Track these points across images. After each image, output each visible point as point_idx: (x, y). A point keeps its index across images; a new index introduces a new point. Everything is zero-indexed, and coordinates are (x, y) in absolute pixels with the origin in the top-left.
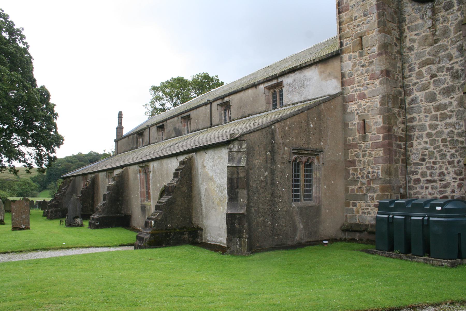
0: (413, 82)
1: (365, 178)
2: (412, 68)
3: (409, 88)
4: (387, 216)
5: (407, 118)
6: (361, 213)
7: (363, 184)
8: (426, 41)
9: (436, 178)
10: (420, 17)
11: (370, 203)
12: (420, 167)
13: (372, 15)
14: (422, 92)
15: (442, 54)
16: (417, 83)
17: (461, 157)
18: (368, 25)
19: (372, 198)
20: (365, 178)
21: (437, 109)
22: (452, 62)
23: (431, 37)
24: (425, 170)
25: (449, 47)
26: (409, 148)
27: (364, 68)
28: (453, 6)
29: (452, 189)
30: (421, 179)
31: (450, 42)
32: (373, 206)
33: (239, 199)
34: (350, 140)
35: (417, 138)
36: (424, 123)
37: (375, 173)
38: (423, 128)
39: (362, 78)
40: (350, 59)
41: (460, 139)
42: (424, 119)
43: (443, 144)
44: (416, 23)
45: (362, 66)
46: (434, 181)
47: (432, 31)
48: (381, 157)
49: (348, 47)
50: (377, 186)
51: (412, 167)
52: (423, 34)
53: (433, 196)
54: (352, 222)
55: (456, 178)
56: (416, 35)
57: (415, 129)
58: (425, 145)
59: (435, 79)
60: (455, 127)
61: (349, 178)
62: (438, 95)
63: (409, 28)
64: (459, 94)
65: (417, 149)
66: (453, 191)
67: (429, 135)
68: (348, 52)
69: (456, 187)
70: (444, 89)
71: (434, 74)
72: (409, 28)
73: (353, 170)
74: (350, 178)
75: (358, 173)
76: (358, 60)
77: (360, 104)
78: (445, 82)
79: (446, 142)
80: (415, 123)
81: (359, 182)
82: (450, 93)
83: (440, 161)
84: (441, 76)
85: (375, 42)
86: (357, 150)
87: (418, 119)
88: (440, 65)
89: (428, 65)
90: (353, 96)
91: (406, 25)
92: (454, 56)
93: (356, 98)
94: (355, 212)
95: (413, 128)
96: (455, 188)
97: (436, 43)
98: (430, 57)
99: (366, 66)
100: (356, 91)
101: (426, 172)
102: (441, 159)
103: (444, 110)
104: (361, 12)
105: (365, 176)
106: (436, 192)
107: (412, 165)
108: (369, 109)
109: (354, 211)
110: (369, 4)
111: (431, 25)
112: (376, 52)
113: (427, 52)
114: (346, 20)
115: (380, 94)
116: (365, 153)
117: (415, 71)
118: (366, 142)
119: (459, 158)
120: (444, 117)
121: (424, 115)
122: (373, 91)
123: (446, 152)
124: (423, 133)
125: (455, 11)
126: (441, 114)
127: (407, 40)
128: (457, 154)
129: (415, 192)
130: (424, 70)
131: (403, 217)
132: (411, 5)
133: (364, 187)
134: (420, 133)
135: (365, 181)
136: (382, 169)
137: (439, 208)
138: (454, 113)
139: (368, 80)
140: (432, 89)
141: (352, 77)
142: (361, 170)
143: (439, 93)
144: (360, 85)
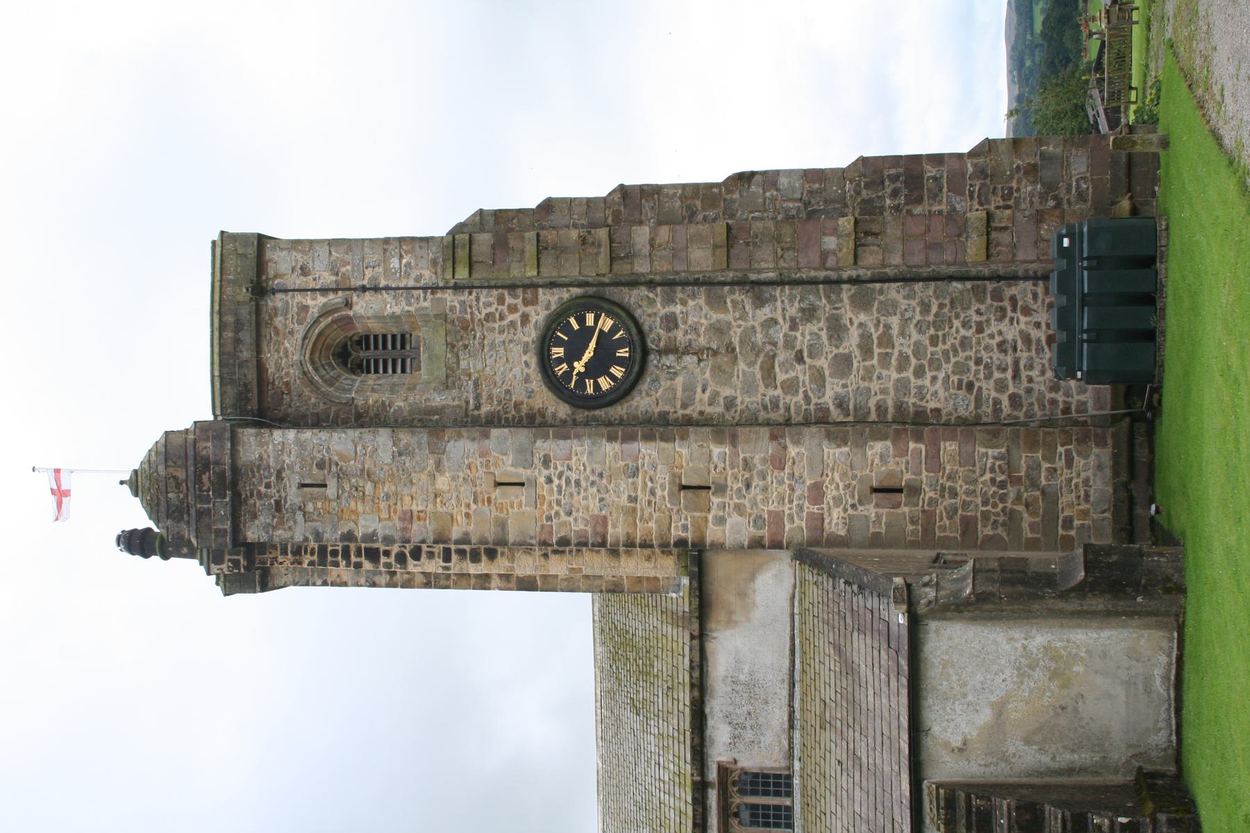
0: (802, 402)
1: (1005, 491)
2: (771, 403)
3: (813, 412)
4: (1085, 345)
5: (876, 420)
6: (1088, 506)
7: (1018, 498)
8: (724, 370)
9: (1009, 359)
10: (672, 379)
11: (1063, 478)
12: (985, 393)
13: (641, 455)
14: (827, 384)
15: (759, 338)
16: (805, 393)
17: (969, 308)
18: (659, 467)
19: (1051, 474)
20: (1005, 491)
21: (869, 354)
22: (780, 320)
23: (719, 359)
24: (992, 382)
25: (749, 324)
26: (941, 418)
27: (754, 484)
28: (674, 313)
29: (1032, 327)
30: (1010, 392)
31: (740, 322)
32: (1069, 471)
33: (1049, 571)
34: (912, 531)
35: (922, 399)
36: (892, 383)
37: (994, 464)
38: (902, 385)
39: (774, 490)
40: (721, 521)
41: (934, 309)
42: (883, 381)
43: (940, 343)
44: (680, 389)
45: (748, 486)
46: (1016, 363)
47: (707, 356)
48: (959, 448)
49: (692, 525)
50: (1023, 461)
51: (985, 412)
52: (708, 375)
53: (1047, 365)
54: (1109, 531)
55: (1012, 319)
56: (704, 391)
57: (902, 403)
58: (940, 382)
59: (805, 354)
60: (909, 318)
61: (1003, 538)
62: (841, 350)
63: (684, 406)
64: (845, 309)
65: (946, 398)
66: (1037, 325)
67: (919, 372)
68: (704, 524)
69: (1028, 319)
70: (830, 337)
71: (796, 356)
72: (684, 406)
73: (984, 526)
74: (1004, 535)
75: (994, 510)
76: (731, 499)
77: (834, 498)
78: (816, 334)
79: (938, 336)
80: (890, 403)
81: (1015, 507)
82: (840, 326)
83: (974, 349)
84: (803, 342)
85: (704, 450)
86: (937, 512)
87: (882, 397)
88: (781, 342)
89: (773, 368)
90: (810, 515)
91: (676, 412)
92: (770, 316)
93: (818, 509)
94: (1087, 522)
95: (899, 407)
96: (1031, 321)
97: (734, 350)
98: (759, 363)
99: (752, 476)
100: (800, 508)
101: (995, 381)
102: (972, 348)
103: (872, 339)
104: (624, 485)
105: (1001, 492)
106: (1038, 360)
107: (979, 411)
108: (850, 473)
109: (1083, 525)
110: (613, 462)
111: (695, 358)
112: (727, 450)
113: (746, 369)
114: (628, 526)
115: (820, 445)
116: (947, 490)
117: (779, 397)
118: (924, 486)
119: (972, 312)
120: (886, 340)
121: (875, 382)
122: (810, 463)
123: (958, 338)
124: (912, 384)
125: (684, 310)
126: (880, 345)
127: (709, 410)
128: (962, 315)
129: (1039, 407)
130: (781, 377)
131: (1086, 309)
132: (637, 399)
133: (1025, 495)
134: (913, 391)
135: (1012, 491)
136: (987, 447)
137: (1066, 242)
138: (882, 318)
139: (782, 474)
140: (825, 361)
141: (766, 516)
142: (985, 503)
143: (837, 347)
144: (790, 496)
